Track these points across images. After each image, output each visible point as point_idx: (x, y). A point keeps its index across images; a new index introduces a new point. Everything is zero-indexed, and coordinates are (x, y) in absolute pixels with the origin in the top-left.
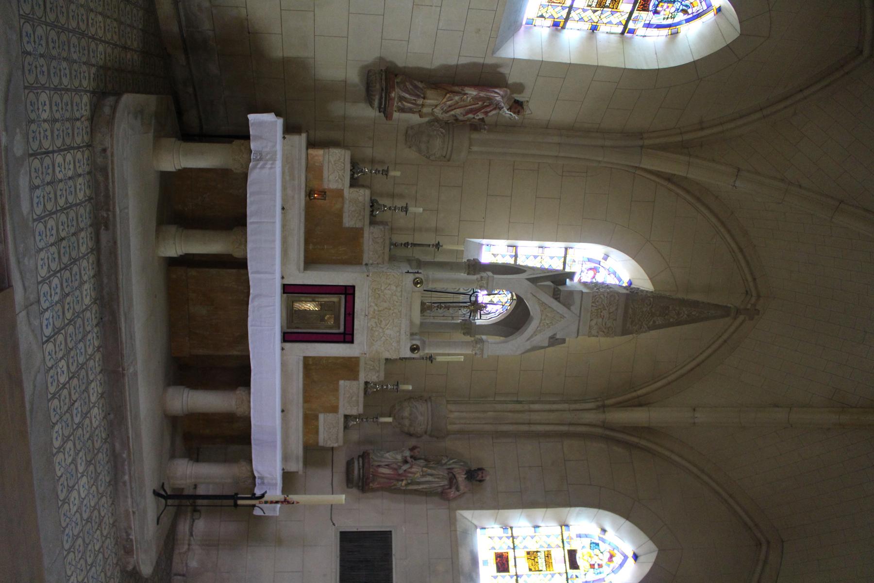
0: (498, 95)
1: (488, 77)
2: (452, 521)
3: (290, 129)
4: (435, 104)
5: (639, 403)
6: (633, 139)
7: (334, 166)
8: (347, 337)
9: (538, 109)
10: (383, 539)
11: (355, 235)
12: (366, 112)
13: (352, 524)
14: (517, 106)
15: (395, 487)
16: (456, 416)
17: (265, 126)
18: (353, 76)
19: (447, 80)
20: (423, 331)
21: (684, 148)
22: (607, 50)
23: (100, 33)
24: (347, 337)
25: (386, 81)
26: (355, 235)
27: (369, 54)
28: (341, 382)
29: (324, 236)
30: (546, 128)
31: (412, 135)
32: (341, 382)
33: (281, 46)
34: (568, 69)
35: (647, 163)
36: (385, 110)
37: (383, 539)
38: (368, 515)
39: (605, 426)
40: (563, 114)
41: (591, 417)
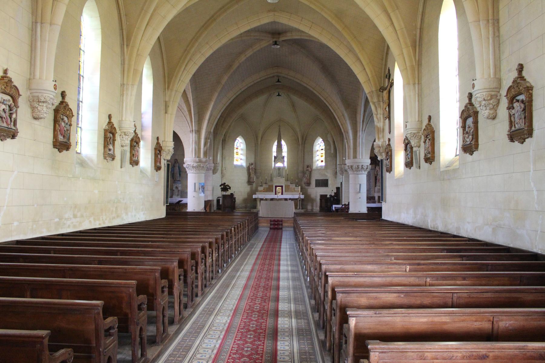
0: (251, 167)
1: (248, 169)
2: (315, 170)
3: (255, 194)
4: (252, 175)
5: (298, 139)
6: (256, 145)
7: (260, 188)
8: (282, 187)
9: (252, 161)
10: (316, 180)
11: (269, 186)
12: (254, 185)
13: (314, 185)
14: (252, 164)
15: (310, 179)
16: (301, 169)
17: (254, 197)
18: (249, 187)
19: (249, 174)
20: (282, 177)
21: (257, 137)
22: (244, 152)
23: (204, 346)
24: (282, 187)
25: (250, 182)
26: (269, 186)
27: (246, 185)
28: (235, 163)
29: (269, 189)
30: (255, 158)
31: (257, 178)
32: (235, 163)
33: (246, 196)
34: (247, 158)
35: (259, 143)
36: (253, 182)
37: (316, 180)
38: (313, 183)
39: (302, 144)
40: (253, 156)
41: (301, 147)
